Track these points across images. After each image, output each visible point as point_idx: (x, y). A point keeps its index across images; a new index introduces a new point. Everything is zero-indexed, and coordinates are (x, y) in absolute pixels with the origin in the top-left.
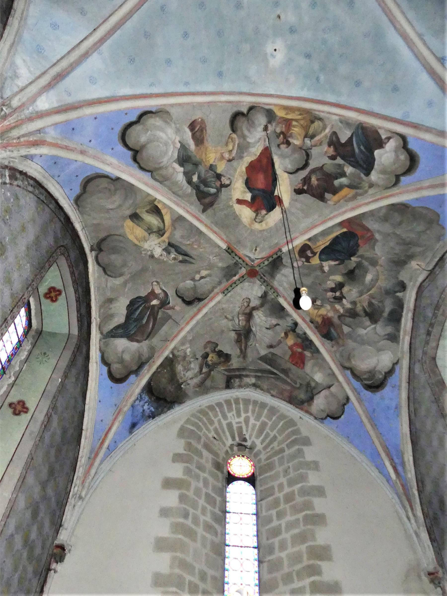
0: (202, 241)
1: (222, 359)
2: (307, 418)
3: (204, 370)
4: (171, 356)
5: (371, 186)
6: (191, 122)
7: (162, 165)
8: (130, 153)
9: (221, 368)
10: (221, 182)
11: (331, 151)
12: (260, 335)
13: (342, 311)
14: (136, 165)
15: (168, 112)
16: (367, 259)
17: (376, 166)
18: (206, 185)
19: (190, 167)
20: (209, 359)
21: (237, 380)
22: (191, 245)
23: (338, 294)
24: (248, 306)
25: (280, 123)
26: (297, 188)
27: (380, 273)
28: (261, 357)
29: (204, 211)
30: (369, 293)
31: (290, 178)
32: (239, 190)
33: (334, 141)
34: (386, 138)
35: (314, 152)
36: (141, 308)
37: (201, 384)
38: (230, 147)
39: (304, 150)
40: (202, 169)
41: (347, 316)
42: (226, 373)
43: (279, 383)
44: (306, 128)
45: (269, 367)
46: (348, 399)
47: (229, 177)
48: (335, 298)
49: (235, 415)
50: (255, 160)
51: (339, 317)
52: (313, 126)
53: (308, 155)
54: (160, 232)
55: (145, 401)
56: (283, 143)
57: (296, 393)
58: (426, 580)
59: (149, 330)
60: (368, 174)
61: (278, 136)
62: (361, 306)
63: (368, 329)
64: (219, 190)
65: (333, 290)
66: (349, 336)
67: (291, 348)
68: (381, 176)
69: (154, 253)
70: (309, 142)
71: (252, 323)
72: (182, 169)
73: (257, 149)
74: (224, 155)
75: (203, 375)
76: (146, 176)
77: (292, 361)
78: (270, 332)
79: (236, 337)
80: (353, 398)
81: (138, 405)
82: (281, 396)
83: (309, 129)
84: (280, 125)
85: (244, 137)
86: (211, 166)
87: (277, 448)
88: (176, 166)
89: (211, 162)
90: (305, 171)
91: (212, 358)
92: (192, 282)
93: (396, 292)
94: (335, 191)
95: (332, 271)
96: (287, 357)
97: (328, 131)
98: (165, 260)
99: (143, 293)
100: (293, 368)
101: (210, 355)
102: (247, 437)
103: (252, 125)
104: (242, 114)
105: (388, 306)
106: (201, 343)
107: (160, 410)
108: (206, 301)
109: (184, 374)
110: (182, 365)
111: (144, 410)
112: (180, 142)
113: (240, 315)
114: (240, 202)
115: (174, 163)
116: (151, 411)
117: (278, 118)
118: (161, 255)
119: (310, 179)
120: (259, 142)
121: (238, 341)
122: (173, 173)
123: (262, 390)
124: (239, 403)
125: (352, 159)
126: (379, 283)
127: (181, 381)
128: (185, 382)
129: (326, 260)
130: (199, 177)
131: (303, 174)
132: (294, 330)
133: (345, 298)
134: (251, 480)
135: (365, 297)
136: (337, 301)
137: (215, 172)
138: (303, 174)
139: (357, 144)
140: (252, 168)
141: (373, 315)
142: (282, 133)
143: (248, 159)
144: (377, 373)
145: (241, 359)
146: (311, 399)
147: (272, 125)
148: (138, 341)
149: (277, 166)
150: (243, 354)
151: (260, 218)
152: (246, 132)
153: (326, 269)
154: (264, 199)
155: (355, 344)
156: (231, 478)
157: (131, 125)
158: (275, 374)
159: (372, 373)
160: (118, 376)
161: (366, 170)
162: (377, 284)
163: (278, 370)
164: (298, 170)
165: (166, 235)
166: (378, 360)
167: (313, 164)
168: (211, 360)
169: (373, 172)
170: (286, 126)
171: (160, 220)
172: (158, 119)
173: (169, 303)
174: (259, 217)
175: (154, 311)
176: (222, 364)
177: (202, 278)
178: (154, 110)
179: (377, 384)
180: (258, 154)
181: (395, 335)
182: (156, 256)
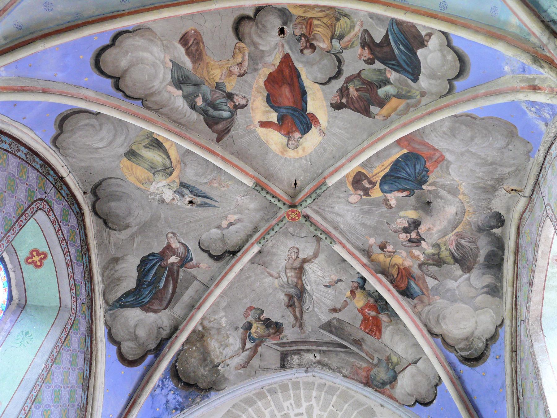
0: (223, 178)
1: (272, 331)
2: (390, 404)
3: (249, 345)
4: (200, 328)
5: (423, 94)
6: (181, 36)
7: (153, 90)
8: (110, 81)
9: (271, 342)
10: (234, 102)
11: (366, 53)
12: (317, 295)
13: (422, 258)
14: (120, 94)
15: (149, 29)
16: (443, 187)
17: (422, 70)
18: (215, 108)
19: (189, 89)
20: (253, 330)
21: (296, 357)
22: (209, 183)
23: (414, 235)
24: (297, 257)
25: (299, 23)
26: (334, 102)
27: (466, 204)
28: (322, 325)
29: (218, 140)
30: (455, 231)
31: (323, 90)
32: (259, 110)
33: (367, 42)
34: (426, 35)
35: (346, 55)
36: (156, 268)
37: (246, 365)
38: (240, 60)
39: (333, 54)
40: (205, 88)
41: (430, 265)
42: (279, 348)
43: (351, 359)
44: (332, 27)
45: (336, 338)
47: (244, 95)
48: (410, 240)
49: (293, 404)
50: (274, 72)
51: (420, 266)
52: (338, 24)
53: (339, 61)
54: (168, 171)
55: (169, 389)
56: (306, 48)
59: (169, 296)
60: (415, 79)
61: (299, 40)
62: (447, 249)
63: (460, 280)
64: (233, 114)
65: (406, 230)
67: (361, 311)
68: (433, 82)
69: (164, 197)
70: (337, 44)
71: (304, 279)
72: (180, 92)
73: (275, 58)
74: (232, 69)
75: (247, 352)
76: (135, 107)
77: (365, 328)
78: (330, 290)
79: (287, 301)
81: (159, 394)
82: (354, 376)
83: (335, 28)
84: (299, 26)
85: (255, 45)
86: (218, 84)
88: (173, 89)
89: (217, 80)
90: (339, 80)
91: (257, 329)
92: (219, 232)
93: (492, 228)
94: (381, 103)
96: (358, 324)
97: (357, 29)
98: (179, 204)
100: (368, 338)
101: (254, 325)
103: (263, 29)
104: (248, 18)
105: (484, 248)
106: (240, 310)
107: (190, 400)
108: (239, 254)
109: (220, 352)
110: (217, 340)
111: (167, 401)
112: (171, 61)
113: (288, 271)
114: (263, 124)
115: (168, 86)
116: (178, 401)
117: (294, 19)
118: (173, 199)
119: (347, 89)
120: (276, 48)
121: (290, 305)
122: (170, 98)
123: (330, 369)
124: (299, 389)
125: (393, 62)
126: (466, 217)
127: (216, 361)
128: (223, 362)
129: (391, 192)
130: (205, 100)
131: (338, 84)
132: (363, 288)
133: (424, 240)
135: (451, 237)
136: (415, 245)
137: (225, 92)
138: (338, 84)
139: (396, 42)
140: (273, 81)
141: (464, 261)
142: (303, 35)
143: (264, 72)
144: (476, 340)
145: (297, 329)
146: (394, 379)
147: (289, 27)
148: (155, 311)
149: (303, 76)
150: (299, 322)
151: (293, 142)
152: (256, 39)
153: (393, 202)
154: (295, 119)
157: (104, 49)
158: (346, 347)
160: (130, 357)
161: (412, 75)
162: (464, 219)
163: (348, 342)
164: (330, 79)
165: (175, 174)
166: (476, 322)
167: (348, 71)
168: (256, 332)
169: (421, 77)
170: (306, 28)
171: (164, 156)
172: (137, 38)
173: (191, 260)
174: (292, 142)
175: (173, 275)
176: (272, 336)
177: (231, 224)
178: (131, 30)
179: (476, 355)
180: (278, 64)
181: (496, 287)
182: (167, 200)
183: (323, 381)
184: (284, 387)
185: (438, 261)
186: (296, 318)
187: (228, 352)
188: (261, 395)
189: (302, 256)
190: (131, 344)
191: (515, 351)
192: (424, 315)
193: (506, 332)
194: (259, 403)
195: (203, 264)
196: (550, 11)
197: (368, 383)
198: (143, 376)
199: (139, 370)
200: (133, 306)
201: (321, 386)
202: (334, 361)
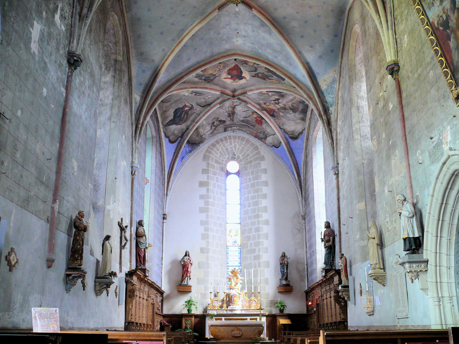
2: (264, 146)
3: (213, 128)
23: (277, 102)
46: (281, 143)
57: (259, 134)
58: (301, 217)
66: (283, 116)
67: (256, 118)
78: (245, 113)
80: (283, 143)
82: (251, 134)
87: (249, 160)
95: (272, 95)
99: (181, 106)
102: (235, 153)
134: (238, 173)
135: (290, 103)
141: (294, 110)
146: (266, 138)
148: (180, 124)
155: (286, 120)
156: (228, 173)
159: (293, 132)
175: (187, 113)
179: (295, 137)
183: (239, 135)
184: (226, 138)
185: (285, 109)
186: (231, 119)
187: (206, 131)
188: (217, 142)
189: (235, 104)
190: (173, 136)
191: (307, 139)
192: (278, 123)
193: (306, 132)
194: (217, 146)
195: (198, 109)
196: (326, 98)
197: (256, 137)
198: (177, 146)
199: (176, 144)
200: (172, 124)
201: (239, 137)
202: (244, 129)
